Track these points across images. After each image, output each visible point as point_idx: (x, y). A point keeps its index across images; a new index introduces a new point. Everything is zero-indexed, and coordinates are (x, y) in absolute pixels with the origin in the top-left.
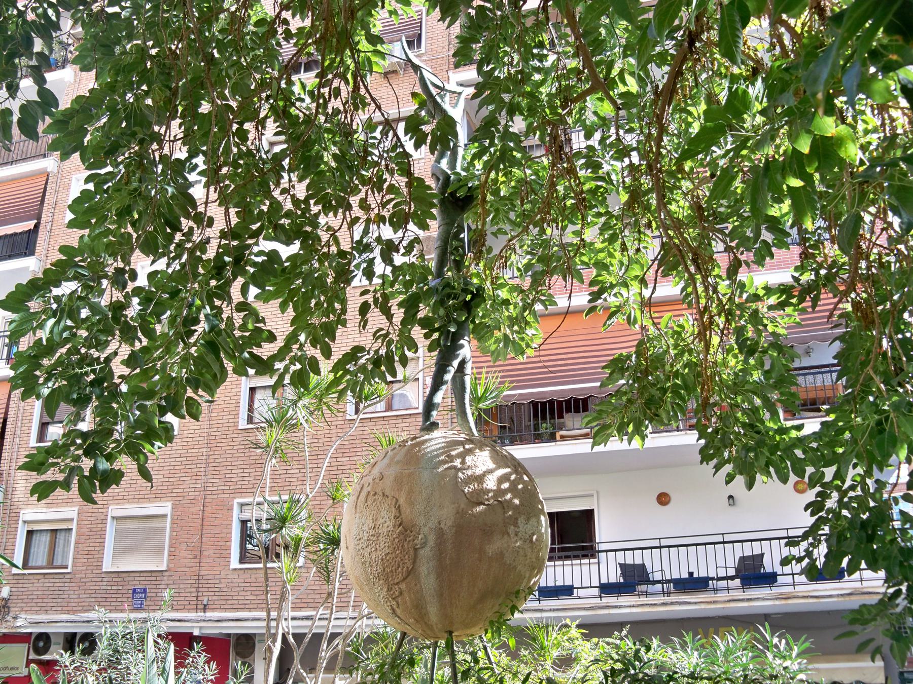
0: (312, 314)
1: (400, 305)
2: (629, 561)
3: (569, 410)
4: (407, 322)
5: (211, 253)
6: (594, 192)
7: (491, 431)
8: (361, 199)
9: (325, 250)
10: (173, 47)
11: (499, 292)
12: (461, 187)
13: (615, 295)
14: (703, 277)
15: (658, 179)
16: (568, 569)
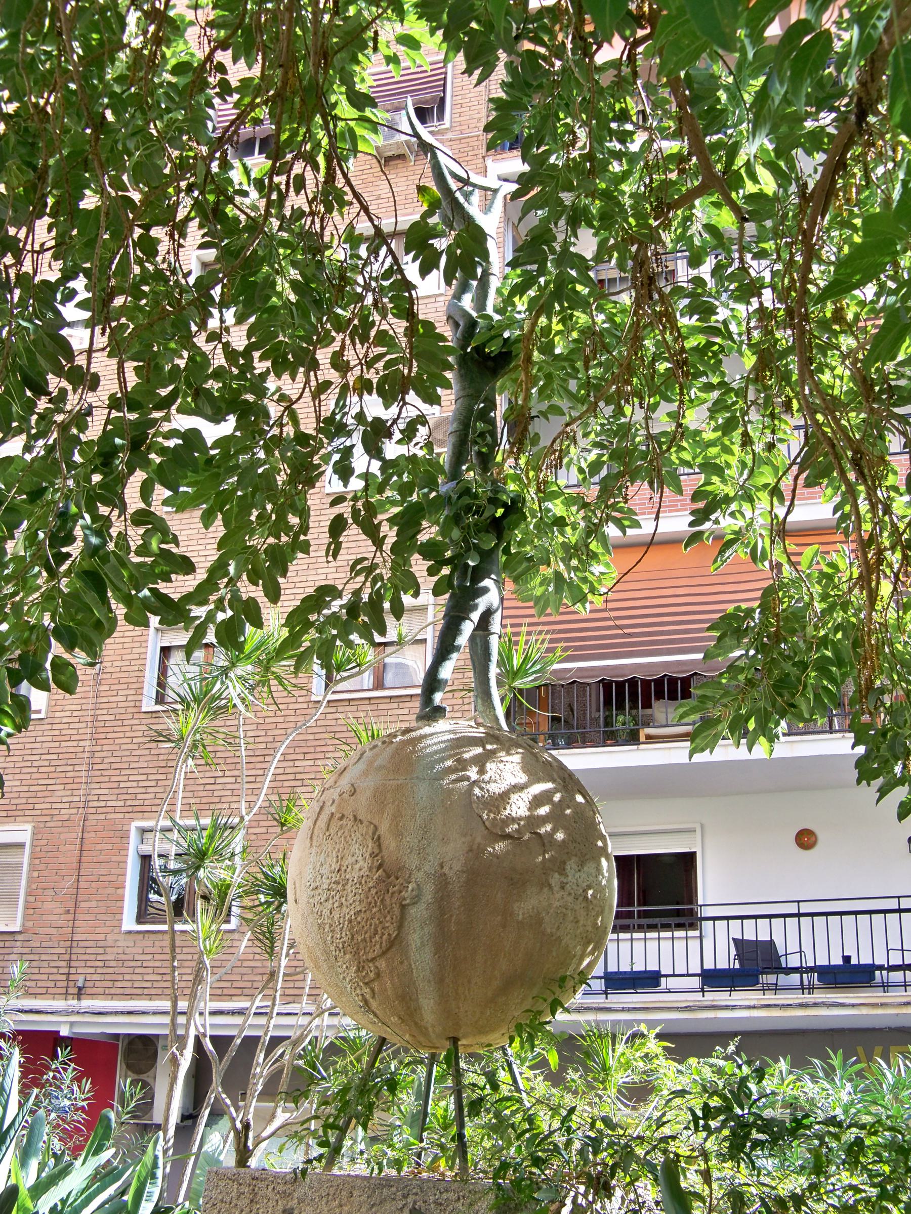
0: (252, 533)
1: (392, 521)
2: (749, 936)
3: (660, 696)
4: (401, 550)
5: (94, 431)
6: (700, 351)
7: (538, 724)
8: (335, 353)
9: (276, 431)
10: (42, 102)
11: (549, 505)
12: (492, 338)
13: (732, 514)
14: (868, 488)
15: (803, 332)
16: (652, 946)
